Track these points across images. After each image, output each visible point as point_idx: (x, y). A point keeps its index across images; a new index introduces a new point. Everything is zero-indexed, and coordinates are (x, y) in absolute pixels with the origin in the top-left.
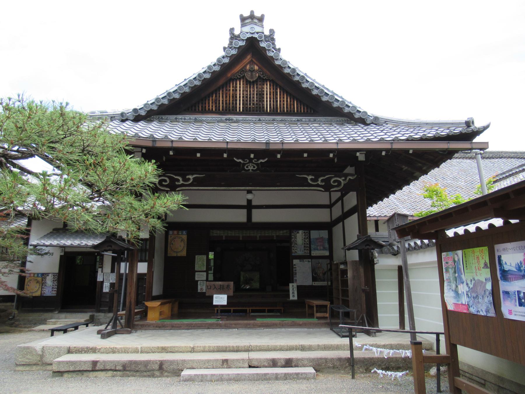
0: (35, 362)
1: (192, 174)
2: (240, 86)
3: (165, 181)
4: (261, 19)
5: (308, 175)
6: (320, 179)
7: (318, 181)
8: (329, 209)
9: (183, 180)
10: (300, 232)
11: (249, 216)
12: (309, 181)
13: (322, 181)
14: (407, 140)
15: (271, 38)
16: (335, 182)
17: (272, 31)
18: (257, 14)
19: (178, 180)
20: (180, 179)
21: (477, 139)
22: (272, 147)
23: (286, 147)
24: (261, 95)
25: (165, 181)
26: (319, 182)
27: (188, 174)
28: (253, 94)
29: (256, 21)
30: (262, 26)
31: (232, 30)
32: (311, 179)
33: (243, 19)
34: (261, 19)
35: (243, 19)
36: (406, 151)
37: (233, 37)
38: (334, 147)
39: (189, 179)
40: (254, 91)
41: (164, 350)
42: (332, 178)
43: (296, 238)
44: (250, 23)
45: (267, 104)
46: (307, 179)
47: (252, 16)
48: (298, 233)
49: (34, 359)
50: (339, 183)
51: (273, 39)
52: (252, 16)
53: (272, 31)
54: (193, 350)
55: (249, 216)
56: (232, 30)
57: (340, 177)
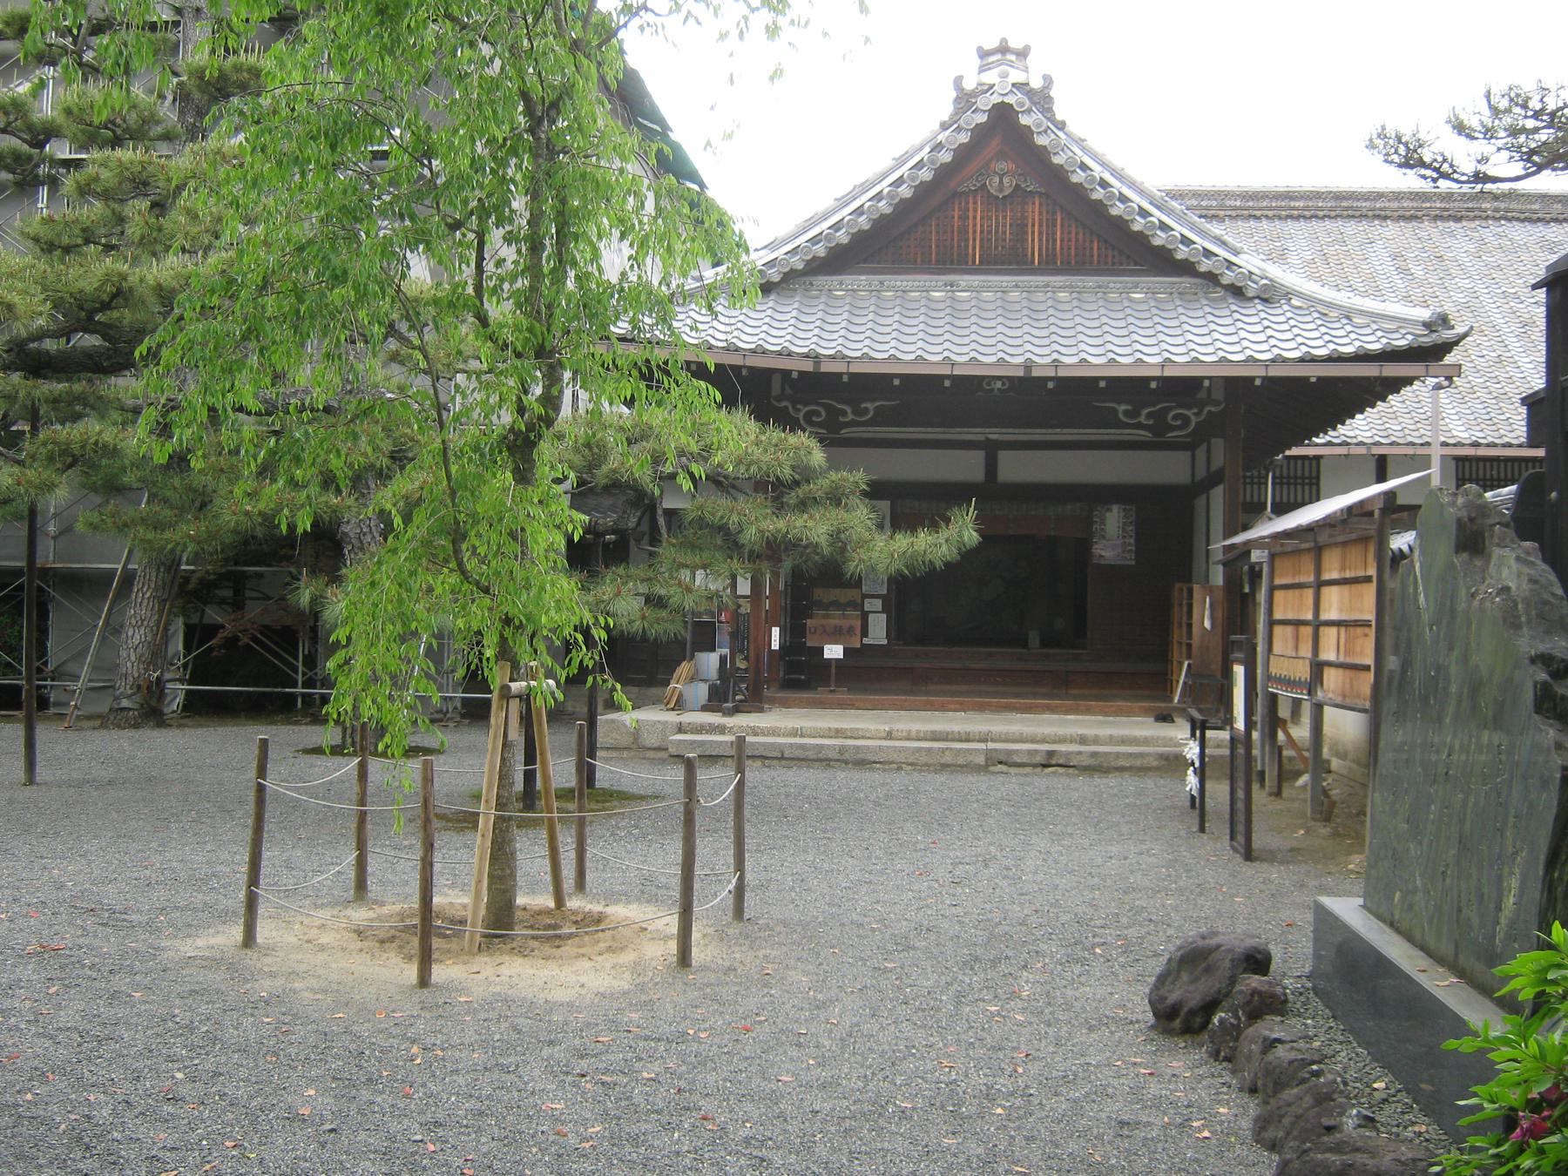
0: (625, 744)
1: (873, 400)
2: (977, 212)
3: (818, 414)
4: (1023, 54)
5: (1119, 403)
6: (1145, 412)
7: (1139, 415)
8: (1189, 453)
9: (854, 413)
10: (1115, 508)
11: (991, 466)
12: (1121, 416)
13: (1149, 416)
14: (1302, 360)
15: (1041, 99)
16: (1175, 418)
17: (1048, 80)
18: (1015, 44)
19: (844, 413)
20: (848, 409)
21: (1449, 359)
22: (1035, 373)
23: (1062, 373)
24: (1021, 227)
25: (818, 414)
26: (1142, 419)
27: (865, 401)
28: (1004, 225)
29: (1013, 58)
30: (1026, 70)
31: (958, 81)
32: (1126, 413)
33: (983, 54)
34: (1023, 54)
35: (983, 54)
36: (1303, 381)
37: (965, 100)
38: (1157, 373)
39: (866, 410)
40: (1005, 217)
41: (839, 733)
42: (1171, 409)
43: (1103, 522)
44: (999, 63)
45: (1035, 246)
46: (1116, 411)
47: (1004, 49)
48: (1109, 510)
49: (625, 740)
50: (1186, 420)
51: (1049, 100)
52: (1004, 49)
53: (1048, 80)
54: (889, 736)
55: (991, 466)
56: (958, 81)
57: (1188, 407)
